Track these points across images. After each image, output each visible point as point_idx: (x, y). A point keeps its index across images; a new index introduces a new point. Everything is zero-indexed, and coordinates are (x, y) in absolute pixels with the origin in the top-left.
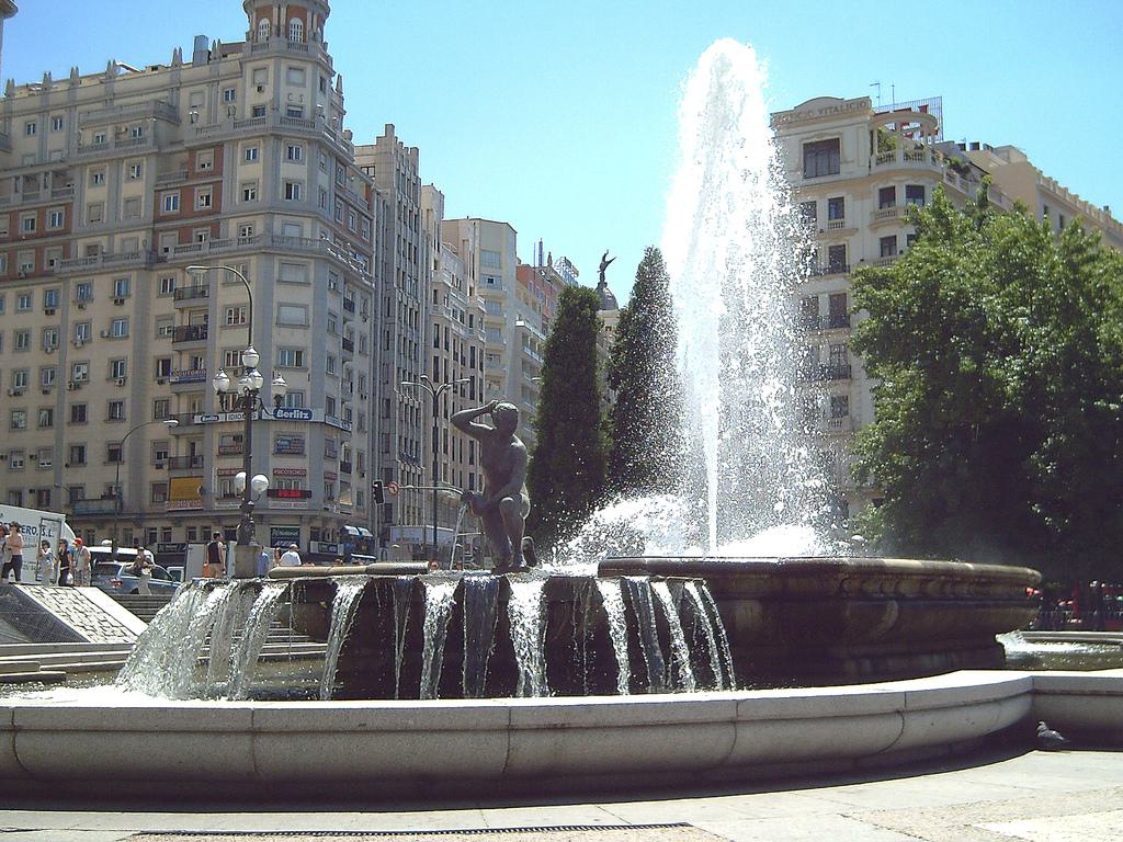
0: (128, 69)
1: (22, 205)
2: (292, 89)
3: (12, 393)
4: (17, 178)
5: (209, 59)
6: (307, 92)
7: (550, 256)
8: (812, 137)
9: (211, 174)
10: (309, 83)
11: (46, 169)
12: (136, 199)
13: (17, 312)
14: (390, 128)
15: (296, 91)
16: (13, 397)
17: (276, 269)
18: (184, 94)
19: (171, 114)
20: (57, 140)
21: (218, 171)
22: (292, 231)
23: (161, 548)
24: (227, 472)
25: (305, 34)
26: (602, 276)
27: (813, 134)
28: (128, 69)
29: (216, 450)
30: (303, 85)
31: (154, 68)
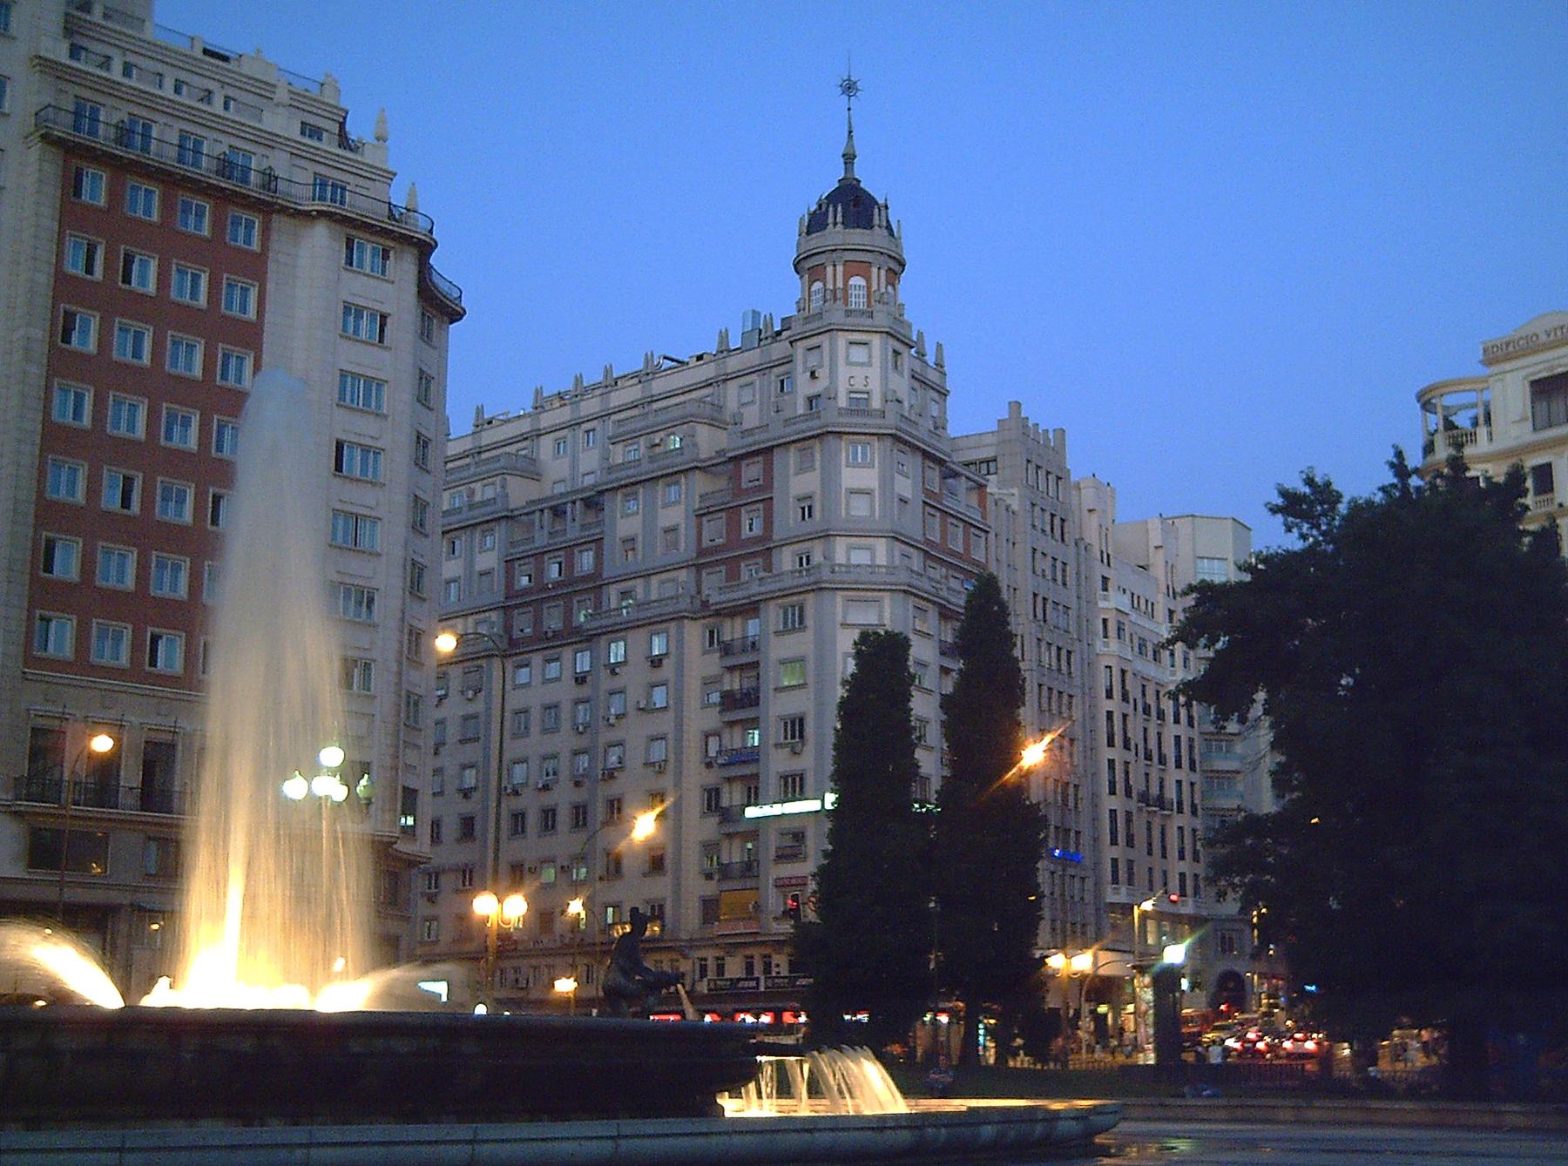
0: (672, 360)
2: (856, 371)
3: (540, 786)
5: (760, 340)
6: (874, 373)
8: (1540, 372)
9: (759, 489)
10: (876, 361)
12: (673, 530)
14: (1016, 406)
15: (859, 373)
16: (542, 793)
17: (839, 610)
21: (768, 484)
22: (861, 558)
23: (712, 986)
24: (786, 882)
25: (869, 296)
27: (1541, 366)
28: (672, 360)
29: (772, 853)
30: (869, 364)
31: (700, 358)
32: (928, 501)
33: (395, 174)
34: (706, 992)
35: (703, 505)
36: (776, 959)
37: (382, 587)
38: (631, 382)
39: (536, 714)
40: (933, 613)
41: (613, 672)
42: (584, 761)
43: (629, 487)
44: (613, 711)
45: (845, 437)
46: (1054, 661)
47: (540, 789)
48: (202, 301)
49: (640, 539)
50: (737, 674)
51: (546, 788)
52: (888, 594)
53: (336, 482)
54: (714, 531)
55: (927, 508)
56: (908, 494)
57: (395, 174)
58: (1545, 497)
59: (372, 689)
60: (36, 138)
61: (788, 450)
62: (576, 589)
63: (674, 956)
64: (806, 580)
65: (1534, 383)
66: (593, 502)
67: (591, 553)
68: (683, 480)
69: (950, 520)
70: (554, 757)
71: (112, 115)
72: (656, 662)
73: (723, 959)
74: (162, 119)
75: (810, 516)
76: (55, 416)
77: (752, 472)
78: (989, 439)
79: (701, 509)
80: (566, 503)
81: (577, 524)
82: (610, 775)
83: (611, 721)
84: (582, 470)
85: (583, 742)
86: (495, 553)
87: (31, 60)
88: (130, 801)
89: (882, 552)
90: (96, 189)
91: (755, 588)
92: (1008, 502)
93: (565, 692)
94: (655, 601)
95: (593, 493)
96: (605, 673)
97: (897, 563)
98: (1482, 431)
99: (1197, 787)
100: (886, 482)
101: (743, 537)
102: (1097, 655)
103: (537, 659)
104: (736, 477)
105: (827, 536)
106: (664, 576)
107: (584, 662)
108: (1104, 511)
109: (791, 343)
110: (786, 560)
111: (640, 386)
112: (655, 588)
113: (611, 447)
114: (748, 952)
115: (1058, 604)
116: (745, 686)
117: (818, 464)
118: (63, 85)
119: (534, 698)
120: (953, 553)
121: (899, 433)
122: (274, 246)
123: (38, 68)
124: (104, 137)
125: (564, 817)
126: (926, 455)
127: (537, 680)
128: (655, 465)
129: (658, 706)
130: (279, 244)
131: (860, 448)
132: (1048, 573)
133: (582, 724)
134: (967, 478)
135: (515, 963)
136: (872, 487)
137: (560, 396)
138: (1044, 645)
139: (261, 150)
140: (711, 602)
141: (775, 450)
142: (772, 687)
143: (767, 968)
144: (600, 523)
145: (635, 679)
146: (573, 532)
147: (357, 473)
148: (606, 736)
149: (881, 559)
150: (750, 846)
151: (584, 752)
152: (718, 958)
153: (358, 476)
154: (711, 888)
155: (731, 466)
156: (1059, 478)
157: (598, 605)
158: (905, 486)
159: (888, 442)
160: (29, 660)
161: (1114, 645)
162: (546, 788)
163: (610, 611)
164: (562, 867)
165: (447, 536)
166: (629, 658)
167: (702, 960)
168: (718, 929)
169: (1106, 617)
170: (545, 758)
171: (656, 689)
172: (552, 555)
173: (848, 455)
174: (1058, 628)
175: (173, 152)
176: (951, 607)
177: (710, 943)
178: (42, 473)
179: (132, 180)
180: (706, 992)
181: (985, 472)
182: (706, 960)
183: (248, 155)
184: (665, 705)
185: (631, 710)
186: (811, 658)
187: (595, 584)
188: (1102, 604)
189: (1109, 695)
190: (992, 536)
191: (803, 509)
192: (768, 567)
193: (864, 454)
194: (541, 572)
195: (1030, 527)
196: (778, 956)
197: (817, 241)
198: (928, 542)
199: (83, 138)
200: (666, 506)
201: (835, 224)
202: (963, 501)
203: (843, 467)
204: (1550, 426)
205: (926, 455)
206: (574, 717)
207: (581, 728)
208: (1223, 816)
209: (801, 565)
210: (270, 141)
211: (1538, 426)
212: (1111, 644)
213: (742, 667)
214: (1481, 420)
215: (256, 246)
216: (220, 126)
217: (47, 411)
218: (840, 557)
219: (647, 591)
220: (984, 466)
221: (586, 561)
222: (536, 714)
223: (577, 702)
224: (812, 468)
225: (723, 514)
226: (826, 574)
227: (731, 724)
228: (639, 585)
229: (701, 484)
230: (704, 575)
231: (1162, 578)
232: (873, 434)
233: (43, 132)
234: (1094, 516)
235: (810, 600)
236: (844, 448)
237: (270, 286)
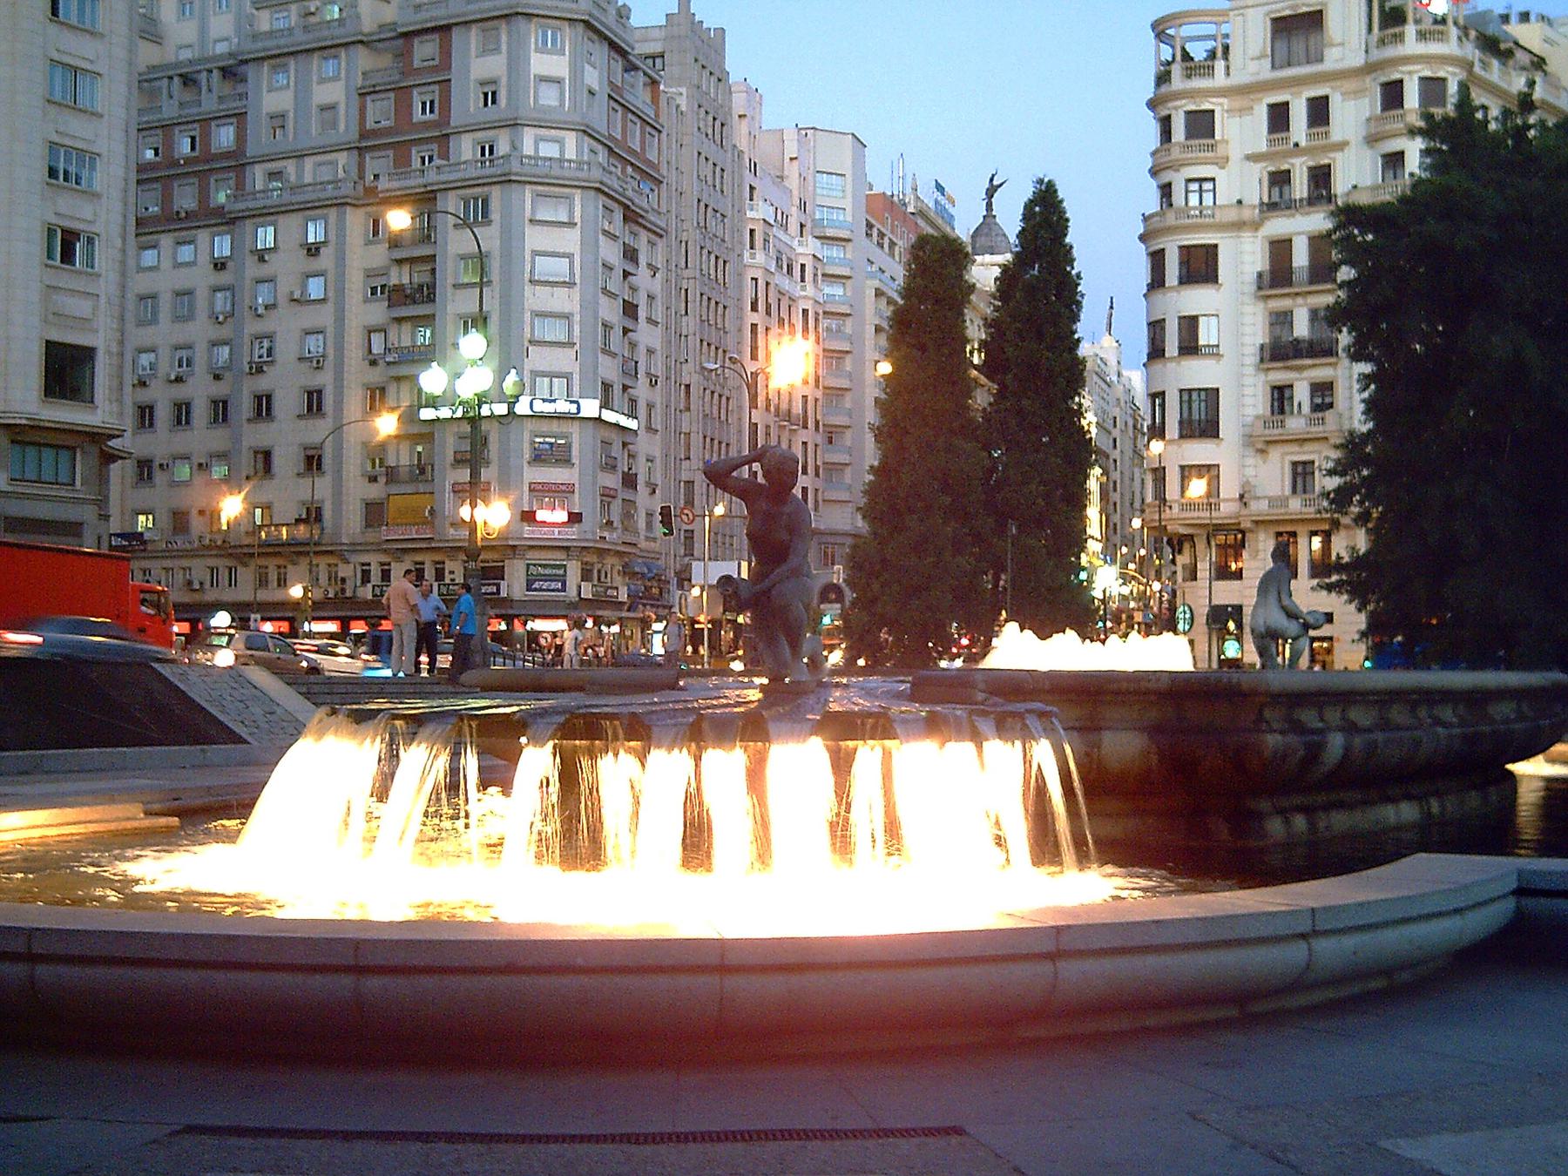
3: (173, 378)
9: (435, 69)
12: (332, 107)
21: (446, 64)
22: (549, 150)
26: (989, 206)
32: (614, 95)
34: (370, 597)
35: (368, 83)
36: (449, 566)
37: (105, 153)
40: (618, 215)
41: (262, 260)
43: (278, 58)
44: (260, 301)
45: (536, 19)
46: (712, 272)
47: (171, 382)
49: (291, 115)
50: (406, 268)
51: (179, 380)
52: (579, 191)
53: (53, 29)
54: (380, 112)
55: (611, 102)
56: (596, 87)
58: (1279, 136)
59: (96, 265)
61: (469, 30)
62: (214, 166)
63: (332, 560)
64: (488, 171)
65: (1275, 21)
66: (232, 71)
67: (231, 129)
68: (343, 55)
69: (630, 116)
72: (313, 250)
73: (389, 564)
75: (494, 102)
77: (424, 50)
78: (657, 34)
79: (364, 88)
80: (199, 72)
81: (215, 96)
83: (260, 312)
85: (225, 332)
89: (571, 145)
91: (432, 176)
92: (678, 102)
93: (201, 278)
94: (310, 185)
96: (250, 261)
97: (586, 158)
98: (1220, 65)
99: (820, 403)
100: (576, 72)
101: (414, 121)
102: (745, 266)
103: (166, 241)
104: (404, 55)
105: (514, 125)
106: (319, 158)
107: (223, 247)
108: (753, 118)
110: (466, 148)
112: (309, 170)
114: (419, 558)
115: (717, 211)
116: (416, 280)
117: (504, 47)
119: (165, 283)
120: (631, 151)
121: (591, 20)
125: (201, 412)
126: (613, 46)
127: (166, 264)
128: (311, 36)
129: (312, 298)
131: (550, 32)
132: (710, 179)
133: (223, 313)
134: (645, 74)
135: (146, 564)
136: (562, 75)
138: (705, 252)
140: (379, 189)
141: (454, 29)
142: (450, 281)
143: (440, 575)
144: (243, 96)
145: (287, 266)
146: (209, 104)
147: (74, 21)
148: (252, 327)
149: (571, 153)
150: (420, 449)
152: (382, 564)
153: (76, 24)
154: (375, 492)
155: (401, 41)
156: (719, 80)
157: (240, 185)
158: (592, 78)
159: (580, 28)
161: (760, 258)
162: (179, 380)
163: (254, 193)
164: (200, 465)
166: (280, 244)
167: (363, 565)
168: (385, 533)
169: (753, 227)
170: (177, 348)
171: (311, 279)
172: (183, 128)
173: (537, 40)
174: (717, 237)
176: (634, 208)
177: (378, 548)
180: (370, 597)
181: (661, 68)
182: (369, 564)
184: (322, 297)
185: (282, 300)
187: (237, 163)
188: (750, 214)
189: (754, 308)
190: (664, 135)
191: (486, 95)
192: (445, 155)
193: (554, 41)
194: (169, 144)
195: (696, 129)
196: (452, 563)
198: (611, 137)
200: (322, 81)
202: (640, 97)
203: (532, 54)
204: (1289, 65)
205: (613, 46)
206: (212, 304)
207: (221, 318)
209: (483, 154)
211: (1277, 64)
212: (757, 256)
213: (412, 261)
214: (1219, 53)
218: (528, 149)
219: (300, 172)
221: (225, 137)
223: (216, 289)
224: (497, 50)
225: (392, 95)
226: (515, 166)
227: (399, 320)
228: (290, 167)
229: (363, 60)
230: (367, 158)
231: (795, 193)
232: (564, 19)
234: (744, 122)
235: (496, 193)
236: (533, 33)
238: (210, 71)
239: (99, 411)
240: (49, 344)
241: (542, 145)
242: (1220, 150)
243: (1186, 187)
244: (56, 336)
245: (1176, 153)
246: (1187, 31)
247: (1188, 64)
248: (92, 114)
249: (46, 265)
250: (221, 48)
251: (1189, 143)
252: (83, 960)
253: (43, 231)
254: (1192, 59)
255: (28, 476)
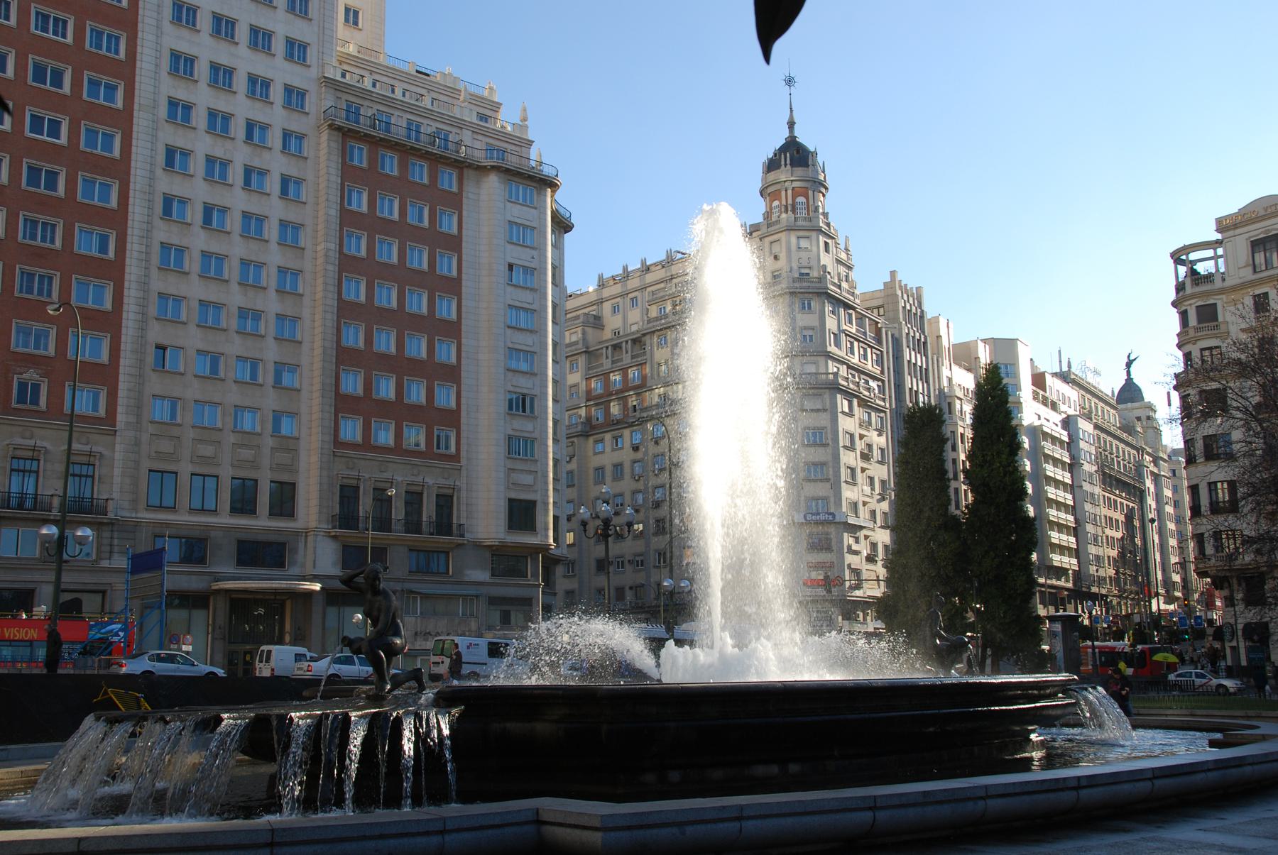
1: (612, 368)
4: (607, 347)
7: (1069, 363)
11: (607, 345)
13: (613, 450)
14: (893, 274)
18: (607, 307)
19: (596, 322)
20: (635, 316)
26: (1128, 373)
33: (533, 142)
38: (657, 268)
39: (609, 470)
41: (657, 443)
42: (640, 497)
48: (426, 223)
57: (533, 142)
60: (325, 126)
66: (638, 341)
70: (621, 495)
71: (367, 111)
74: (397, 113)
76: (345, 296)
82: (657, 505)
84: (630, 322)
86: (579, 374)
87: (319, 79)
88: (400, 527)
90: (360, 157)
93: (626, 455)
95: (639, 335)
96: (651, 445)
109: (761, 239)
111: (664, 269)
113: (649, 307)
118: (340, 94)
122: (465, 188)
123: (323, 84)
124: (363, 126)
130: (469, 188)
137: (613, 278)
139: (454, 130)
151: (640, 491)
160: (337, 443)
165: (570, 359)
175: (404, 132)
178: (339, 330)
179: (382, 151)
183: (447, 134)
186: (576, 472)
197: (772, 176)
199: (352, 126)
201: (786, 165)
206: (633, 470)
208: (402, 609)
210: (460, 124)
215: (455, 189)
216: (428, 114)
217: (340, 293)
220: (876, 311)
222: (609, 470)
233: (330, 122)
237: (465, 213)
238: (627, 342)
239: (539, 535)
240: (511, 501)
241: (806, 366)
242: (1223, 328)
243: (1202, 354)
244: (513, 495)
245: (1192, 333)
246: (1193, 256)
247: (1196, 277)
248: (531, 374)
249: (508, 458)
250: (634, 328)
251: (1201, 325)
252: (649, 826)
253: (505, 439)
254: (1199, 273)
255: (441, 571)
